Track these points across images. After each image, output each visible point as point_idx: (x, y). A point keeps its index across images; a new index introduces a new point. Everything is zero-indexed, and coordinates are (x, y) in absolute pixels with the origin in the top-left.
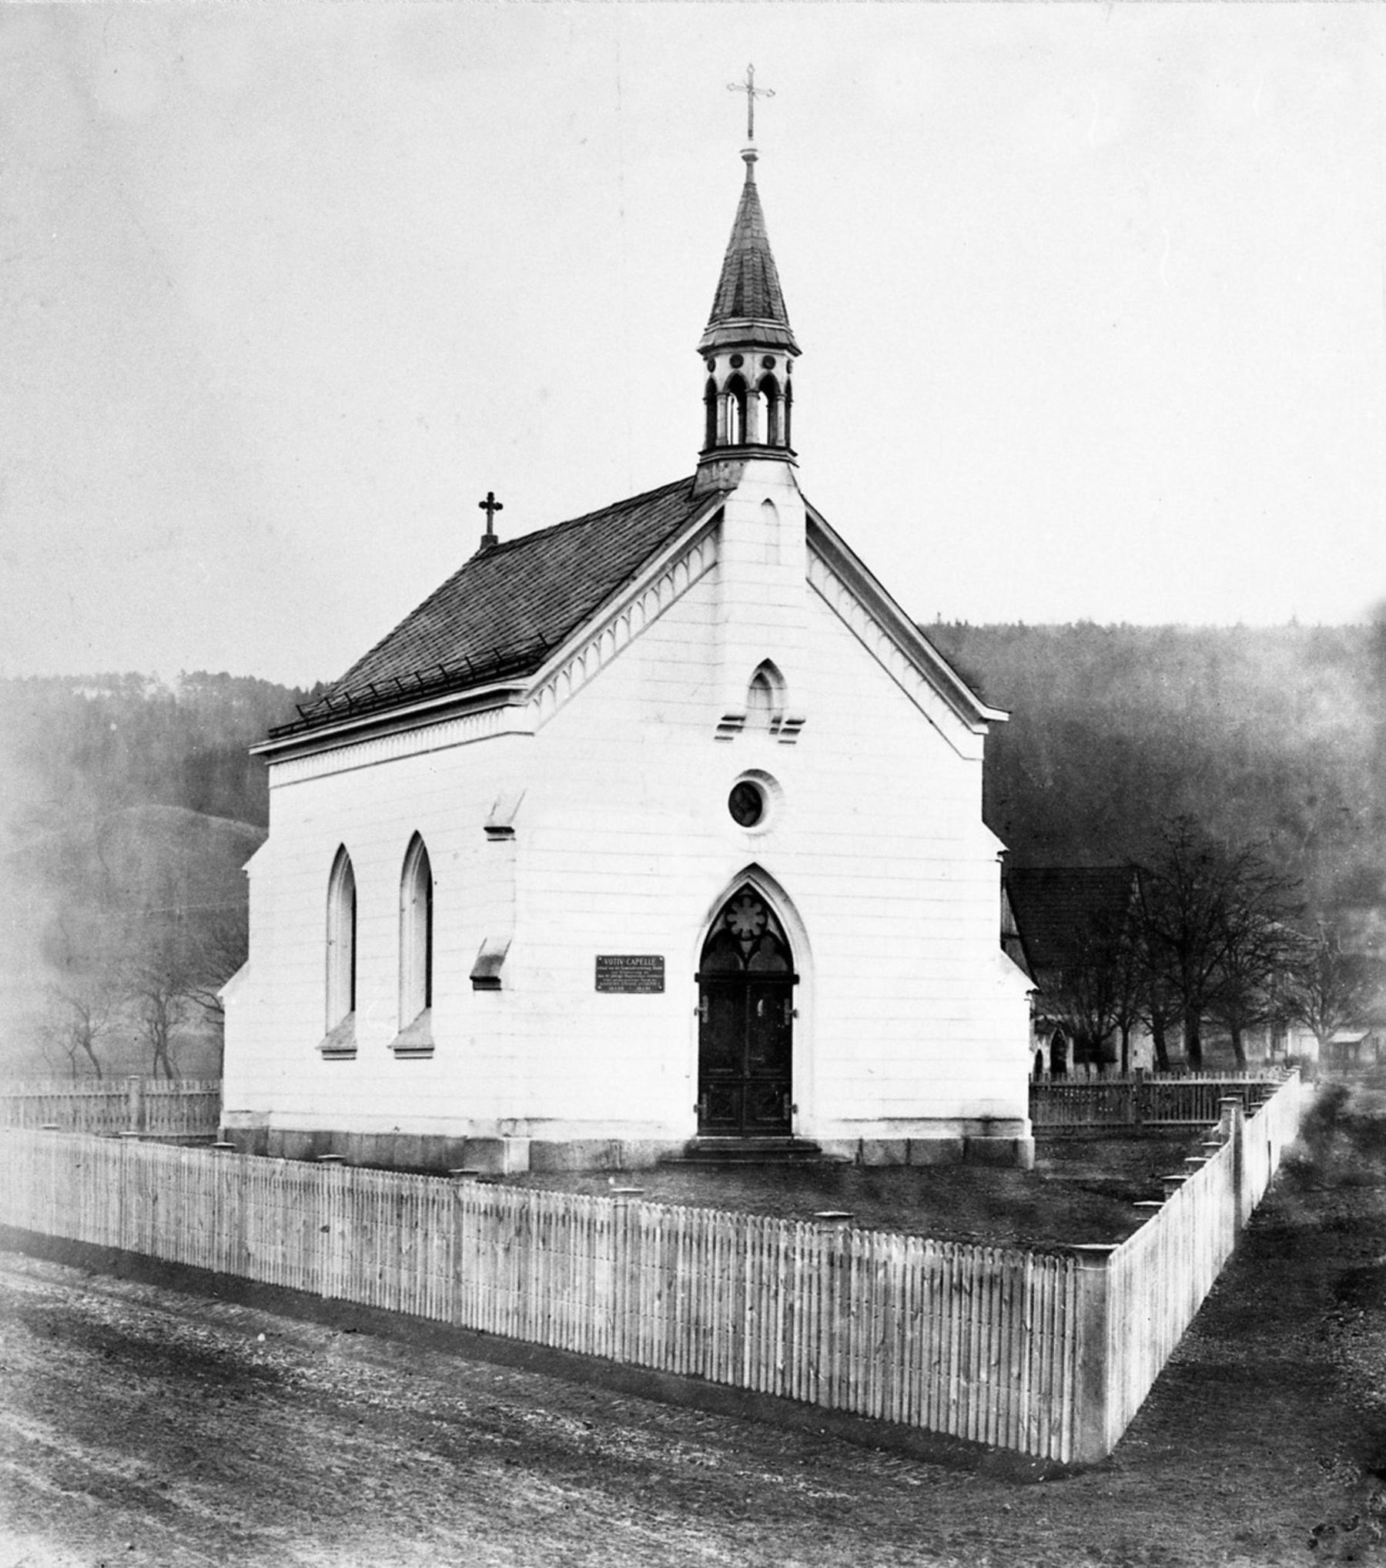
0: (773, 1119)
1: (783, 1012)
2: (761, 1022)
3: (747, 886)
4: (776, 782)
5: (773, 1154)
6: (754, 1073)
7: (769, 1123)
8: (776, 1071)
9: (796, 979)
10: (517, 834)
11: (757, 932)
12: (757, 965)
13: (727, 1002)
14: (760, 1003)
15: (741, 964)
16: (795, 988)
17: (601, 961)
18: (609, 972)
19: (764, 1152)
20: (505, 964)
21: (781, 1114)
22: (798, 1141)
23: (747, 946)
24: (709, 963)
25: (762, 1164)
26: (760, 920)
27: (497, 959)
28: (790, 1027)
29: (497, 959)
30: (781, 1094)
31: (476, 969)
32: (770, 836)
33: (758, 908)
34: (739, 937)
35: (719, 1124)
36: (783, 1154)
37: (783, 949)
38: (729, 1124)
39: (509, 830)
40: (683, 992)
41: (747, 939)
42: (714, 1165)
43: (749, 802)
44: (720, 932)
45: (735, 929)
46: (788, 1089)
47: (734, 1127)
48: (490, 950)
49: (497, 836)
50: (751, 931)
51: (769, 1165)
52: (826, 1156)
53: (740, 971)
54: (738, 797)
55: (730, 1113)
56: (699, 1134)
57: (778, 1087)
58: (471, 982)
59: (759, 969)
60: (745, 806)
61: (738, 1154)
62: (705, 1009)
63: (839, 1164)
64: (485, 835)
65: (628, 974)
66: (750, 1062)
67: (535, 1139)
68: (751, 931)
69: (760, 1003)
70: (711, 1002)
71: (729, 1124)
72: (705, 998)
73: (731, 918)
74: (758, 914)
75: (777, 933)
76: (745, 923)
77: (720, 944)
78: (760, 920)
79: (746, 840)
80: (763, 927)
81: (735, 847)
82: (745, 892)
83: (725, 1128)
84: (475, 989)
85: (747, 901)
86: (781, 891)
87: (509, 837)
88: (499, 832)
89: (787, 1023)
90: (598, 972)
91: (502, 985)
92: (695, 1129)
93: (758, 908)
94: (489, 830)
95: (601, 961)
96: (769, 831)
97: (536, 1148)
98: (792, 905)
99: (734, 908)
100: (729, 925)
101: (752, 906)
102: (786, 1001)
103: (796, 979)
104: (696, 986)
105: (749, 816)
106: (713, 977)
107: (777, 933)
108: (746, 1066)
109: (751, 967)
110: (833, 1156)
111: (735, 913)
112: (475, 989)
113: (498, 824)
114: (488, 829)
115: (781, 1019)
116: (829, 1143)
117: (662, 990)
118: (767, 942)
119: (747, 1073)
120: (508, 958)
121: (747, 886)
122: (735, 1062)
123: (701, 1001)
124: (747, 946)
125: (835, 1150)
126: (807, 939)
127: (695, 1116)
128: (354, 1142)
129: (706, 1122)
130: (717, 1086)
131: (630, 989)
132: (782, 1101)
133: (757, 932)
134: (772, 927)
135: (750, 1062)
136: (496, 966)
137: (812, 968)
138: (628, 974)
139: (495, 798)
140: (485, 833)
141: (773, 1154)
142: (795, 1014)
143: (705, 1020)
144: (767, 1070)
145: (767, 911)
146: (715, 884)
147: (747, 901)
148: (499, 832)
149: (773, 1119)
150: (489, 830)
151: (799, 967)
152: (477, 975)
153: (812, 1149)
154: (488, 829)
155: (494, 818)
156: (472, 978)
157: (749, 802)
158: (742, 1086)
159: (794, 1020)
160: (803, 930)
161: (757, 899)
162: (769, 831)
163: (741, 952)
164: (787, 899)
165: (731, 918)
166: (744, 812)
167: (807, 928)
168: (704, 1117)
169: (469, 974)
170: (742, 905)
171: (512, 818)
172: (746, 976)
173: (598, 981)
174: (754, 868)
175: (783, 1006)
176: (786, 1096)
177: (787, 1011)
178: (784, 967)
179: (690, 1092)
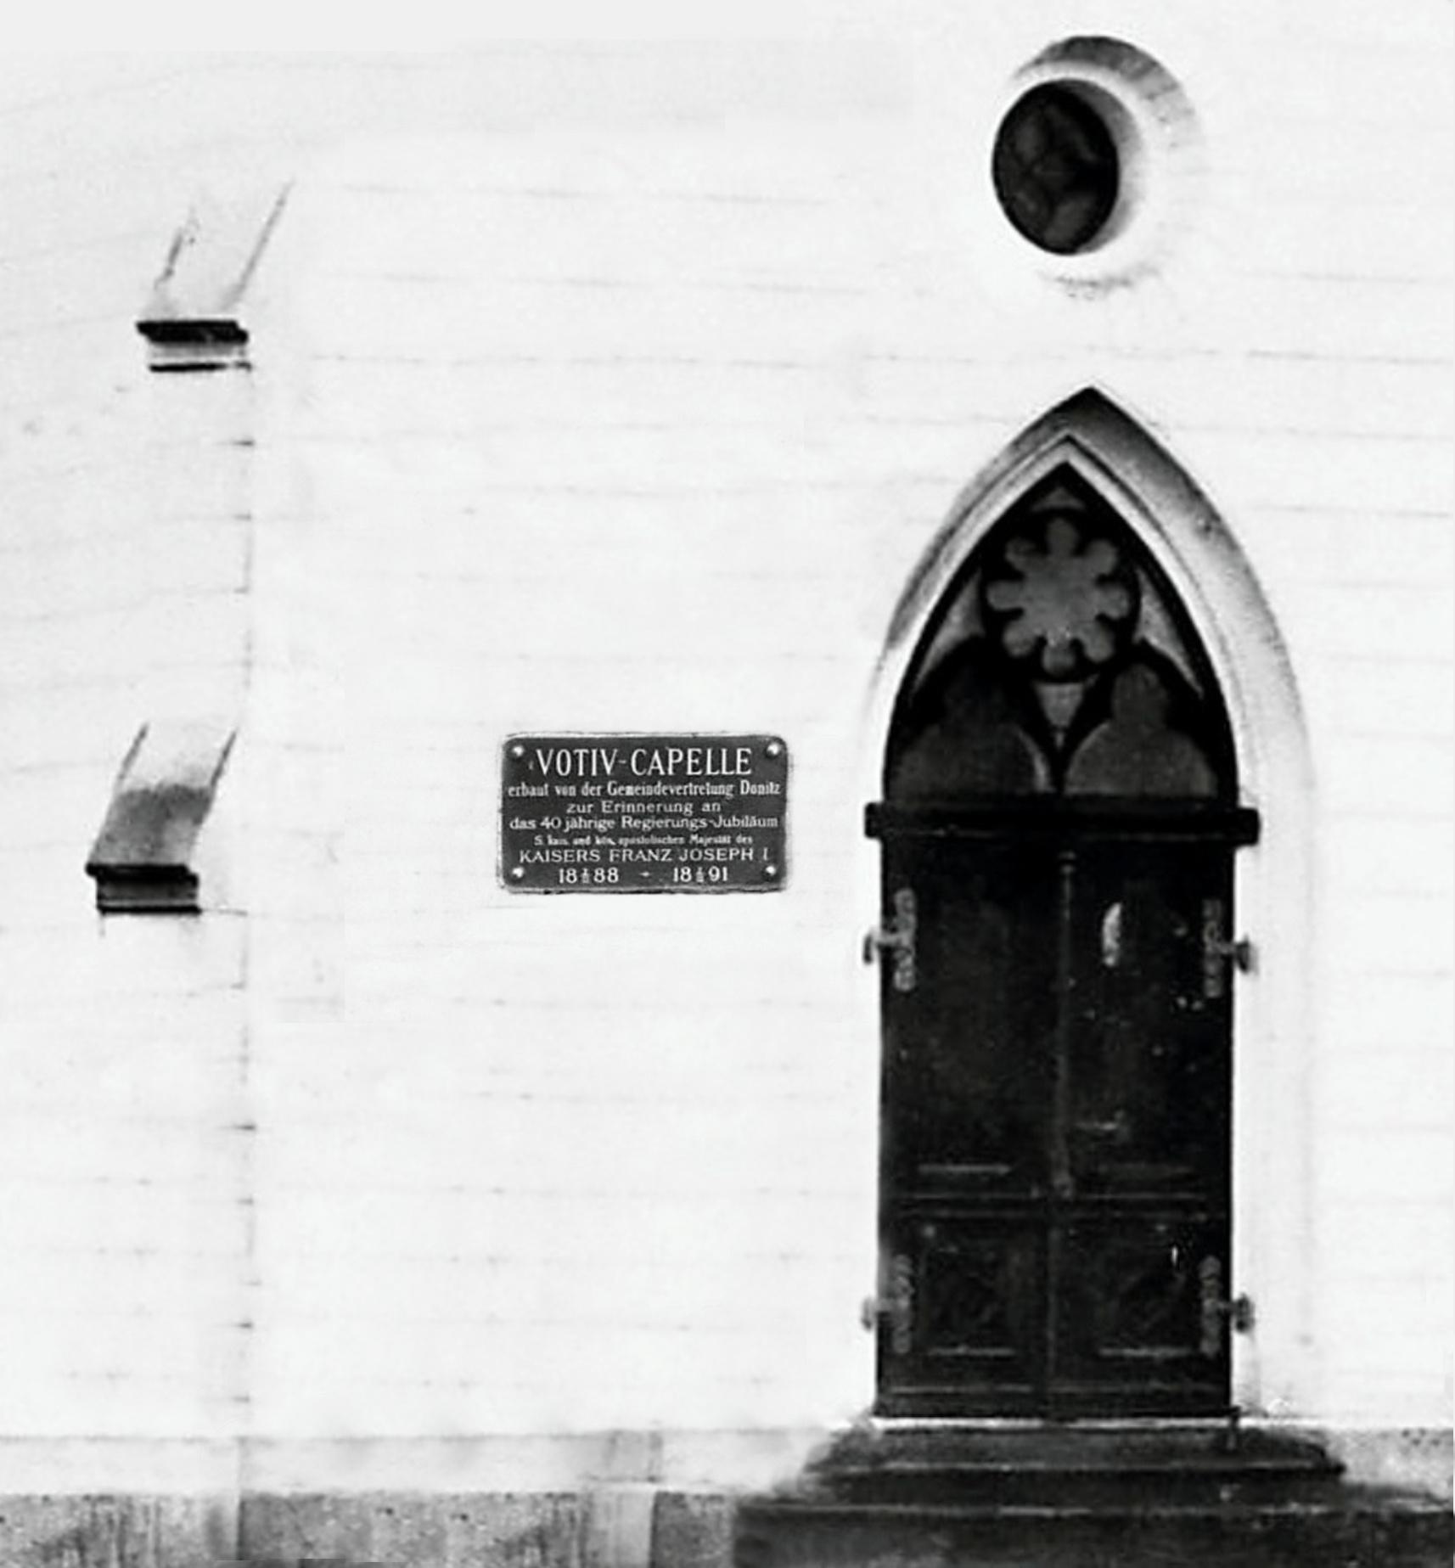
0: (1160, 1353)
1: (1197, 950)
2: (1115, 987)
3: (1064, 476)
4: (1172, 86)
5: (1159, 1483)
6: (1087, 1181)
7: (1144, 1368)
8: (1168, 1170)
9: (1247, 827)
10: (255, 349)
11: (1098, 648)
12: (1097, 774)
13: (988, 912)
14: (1113, 917)
15: (1041, 770)
16: (1243, 858)
17: (525, 762)
18: (555, 806)
19: (1126, 1478)
20: (210, 821)
21: (1193, 1335)
22: (1255, 1433)
23: (1061, 701)
24: (916, 762)
25: (1120, 1523)
26: (1114, 604)
27: (185, 803)
28: (1223, 1007)
29: (185, 803)
30: (1192, 1261)
31: (108, 838)
32: (1148, 285)
33: (1105, 558)
34: (1031, 667)
35: (958, 1369)
36: (1199, 1484)
37: (1199, 715)
38: (996, 1370)
39: (230, 334)
40: (838, 876)
41: (1061, 677)
42: (938, 1524)
43: (1072, 159)
44: (961, 652)
45: (1016, 638)
46: (1215, 1238)
47: (1010, 1381)
48: (158, 768)
49: (184, 356)
50: (1076, 646)
51: (1145, 1524)
52: (1360, 1490)
53: (1035, 798)
54: (1028, 140)
55: (997, 1331)
56: (880, 1410)
57: (1179, 1234)
58: (91, 884)
59: (1106, 788)
60: (1055, 174)
61: (1026, 1486)
62: (905, 938)
63: (1405, 1520)
64: (143, 350)
65: (614, 813)
66: (1072, 1137)
67: (671, 1487)
68: (1076, 646)
69: (1113, 917)
70: (927, 915)
71: (996, 1370)
72: (904, 898)
73: (1001, 597)
74: (1103, 581)
75: (1175, 654)
76: (1056, 615)
77: (958, 693)
78: (1114, 604)
79: (1057, 294)
80: (1123, 629)
81: (1024, 329)
82: (1057, 499)
83: (980, 1387)
84: (104, 910)
85: (1062, 534)
86: (1192, 494)
87: (230, 357)
88: (191, 340)
89: (1212, 990)
90: (511, 807)
91: (204, 897)
92: (865, 1391)
93: (1105, 558)
94: (158, 331)
95: (525, 762)
96: (1147, 269)
97: (674, 1513)
98: (1232, 546)
99: (1015, 557)
100: (994, 621)
101: (1080, 550)
102: (1210, 909)
103: (1247, 827)
104: (872, 850)
105: (1070, 213)
106: (937, 818)
107: (1175, 654)
108: (1058, 1152)
109: (1077, 783)
110: (1387, 1492)
111: (1015, 576)
112: (104, 910)
113: (190, 312)
114: (146, 328)
115: (1191, 979)
116: (1366, 1441)
117: (774, 882)
118: (1140, 685)
119: (1062, 1179)
120: (225, 795)
121: (1064, 476)
122: (1019, 1141)
123: (888, 910)
124: (1061, 701)
125: (1395, 1469)
126: (1287, 673)
127: (869, 1341)
128: (176, 1514)
129: (912, 1354)
130: (950, 1228)
131: (644, 877)
132: (1194, 1284)
133: (1098, 648)
134: (1155, 631)
135: (1072, 1137)
136: (180, 826)
137: (1309, 782)
138: (614, 813)
139: (177, 219)
140: (141, 341)
141: (1159, 1483)
142: (1242, 957)
143: (904, 980)
144: (1137, 1169)
145: (1136, 566)
146: (947, 460)
147: (1062, 534)
148: (191, 340)
149: (1160, 1353)
150: (158, 331)
151: (1257, 783)
152: (111, 859)
153: (1307, 1464)
154: (146, 328)
155: (175, 287)
156: (92, 869)
157: (1072, 159)
158: (1043, 1229)
159: (1240, 980)
160: (1275, 641)
161: (1100, 523)
162: (1147, 269)
163: (1039, 726)
164: (1212, 525)
165: (1001, 597)
166: (1050, 199)
167: (1289, 637)
168: (901, 1345)
169: (83, 860)
170: (1042, 548)
171: (239, 290)
172: (1059, 816)
173: (513, 843)
174: (1088, 408)
175: (1196, 927)
176: (1210, 1266)
177: (1211, 945)
178: (1203, 783)
179: (840, 1259)
